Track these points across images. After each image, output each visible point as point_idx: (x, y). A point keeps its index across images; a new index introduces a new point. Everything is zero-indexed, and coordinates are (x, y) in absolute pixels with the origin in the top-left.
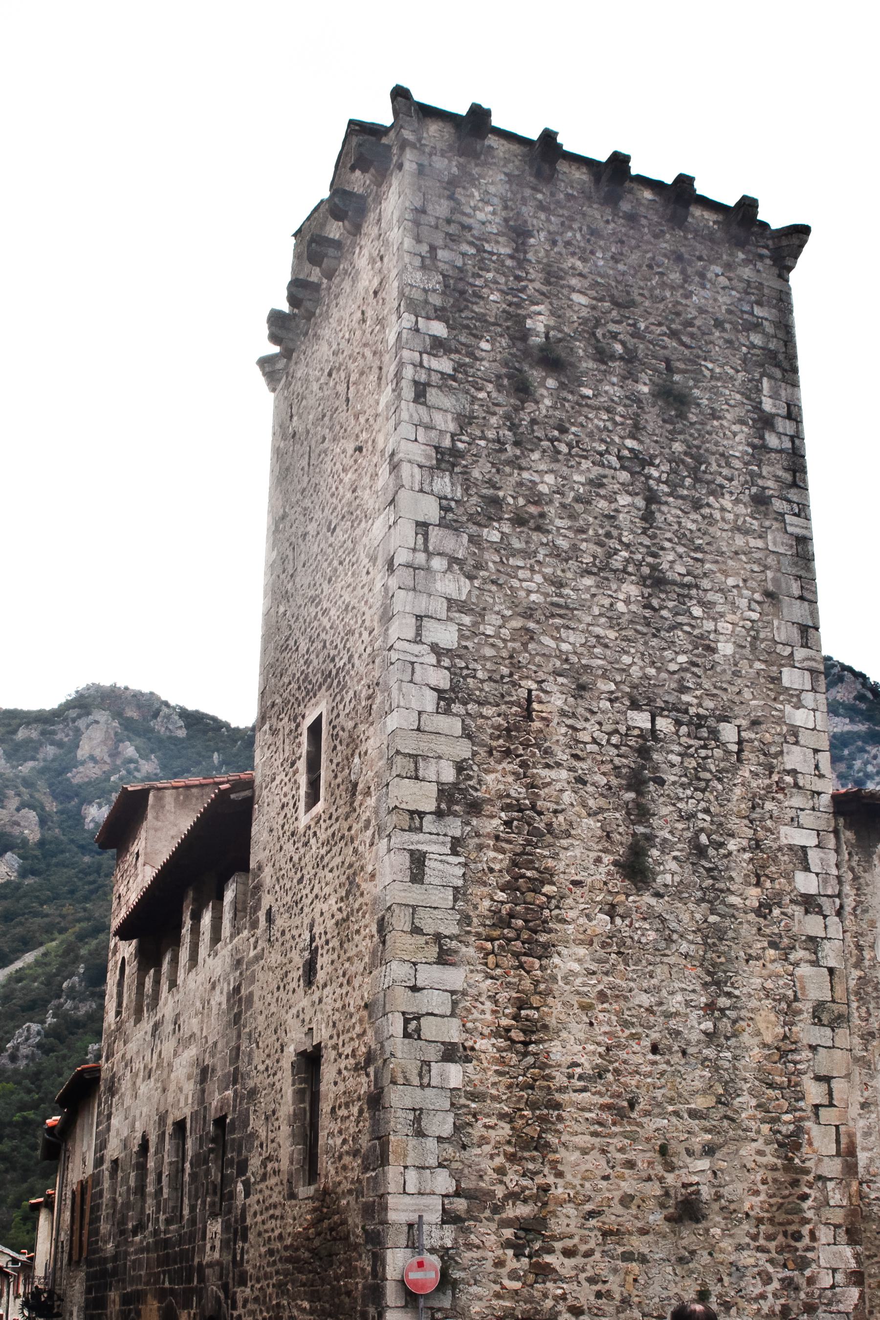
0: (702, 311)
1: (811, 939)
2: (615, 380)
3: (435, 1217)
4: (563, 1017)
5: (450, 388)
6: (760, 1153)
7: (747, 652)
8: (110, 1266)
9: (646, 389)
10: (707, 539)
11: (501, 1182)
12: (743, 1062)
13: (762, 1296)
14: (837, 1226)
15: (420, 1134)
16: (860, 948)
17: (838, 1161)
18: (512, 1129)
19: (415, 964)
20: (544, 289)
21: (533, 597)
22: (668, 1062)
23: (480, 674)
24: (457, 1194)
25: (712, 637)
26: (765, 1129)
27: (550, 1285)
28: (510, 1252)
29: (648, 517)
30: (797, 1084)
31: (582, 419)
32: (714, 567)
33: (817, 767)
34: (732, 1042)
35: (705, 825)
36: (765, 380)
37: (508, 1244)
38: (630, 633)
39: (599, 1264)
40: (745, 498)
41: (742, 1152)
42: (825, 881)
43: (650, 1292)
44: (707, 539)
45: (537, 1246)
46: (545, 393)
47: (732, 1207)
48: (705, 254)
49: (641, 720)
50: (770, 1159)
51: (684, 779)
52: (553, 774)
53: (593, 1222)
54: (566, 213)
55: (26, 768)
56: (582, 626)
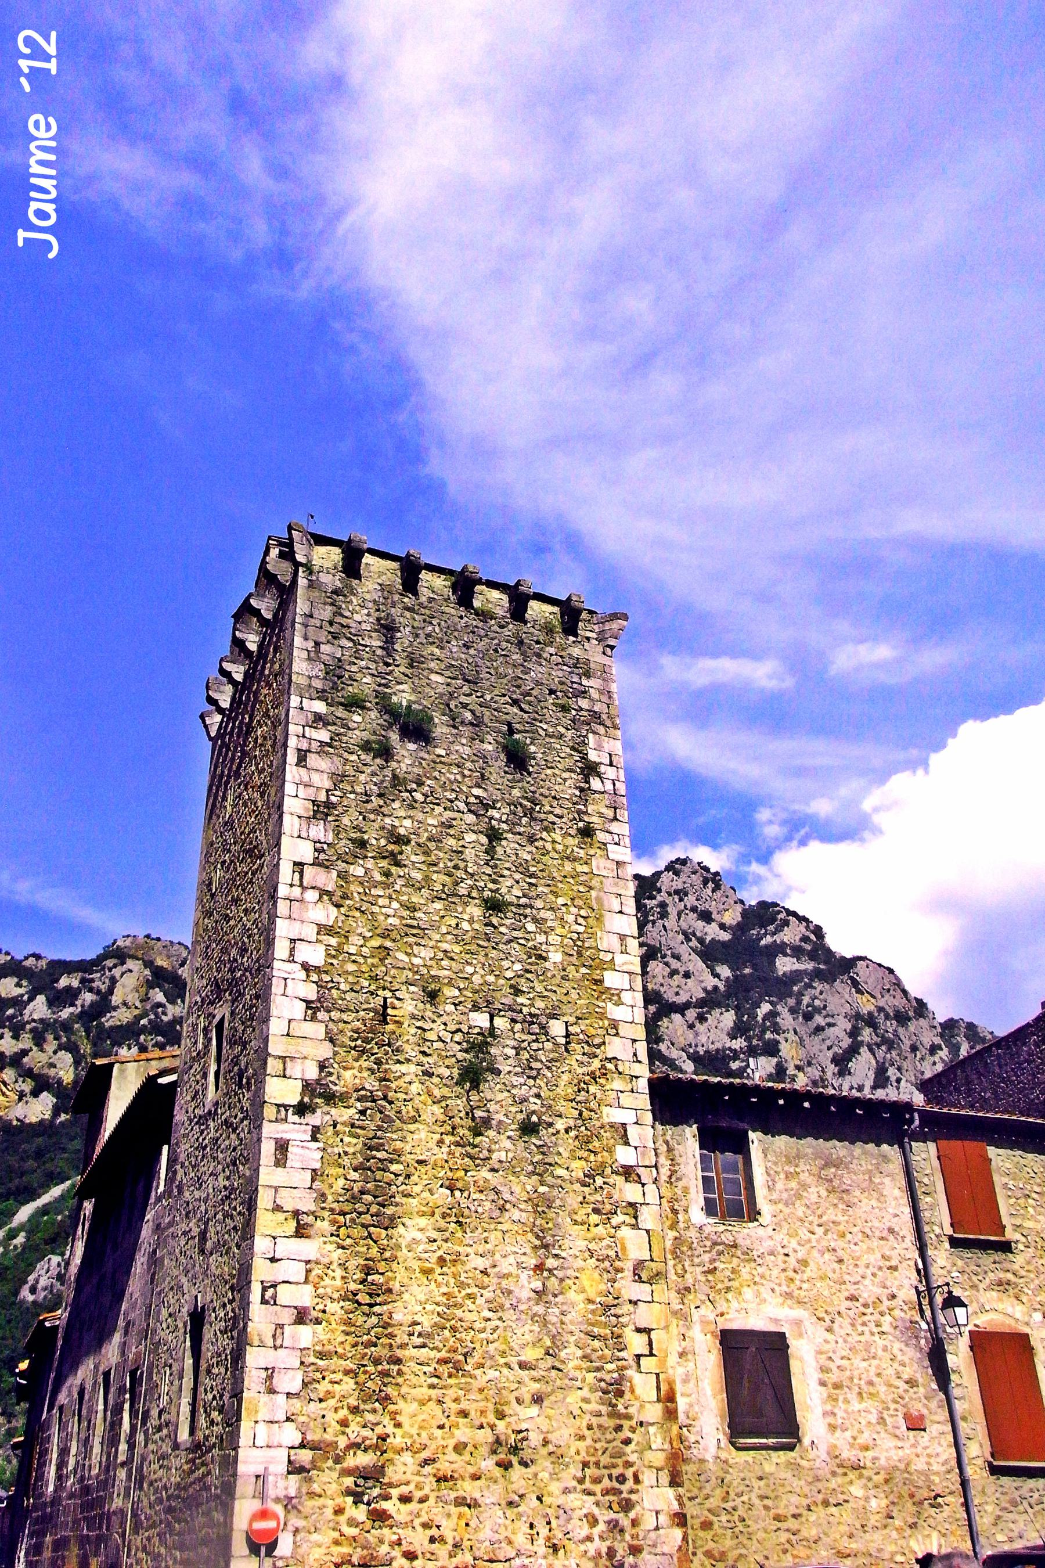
0: (538, 683)
1: (632, 1205)
2: (464, 741)
3: (283, 1467)
4: (406, 1281)
5: (327, 753)
6: (586, 1401)
7: (574, 959)
9: (490, 748)
10: (541, 866)
11: (343, 1433)
12: (569, 1317)
13: (589, 1539)
14: (658, 1470)
15: (272, 1391)
16: (675, 1212)
17: (659, 1407)
18: (357, 1383)
19: (274, 1238)
20: (408, 672)
21: (391, 920)
22: (500, 1319)
23: (342, 987)
24: (302, 1446)
25: (544, 947)
26: (590, 1377)
27: (386, 1531)
28: (350, 1500)
29: (490, 851)
30: (619, 1336)
31: (436, 774)
32: (546, 890)
33: (635, 1054)
34: (560, 1299)
35: (536, 1108)
36: (590, 735)
37: (349, 1492)
38: (473, 948)
39: (433, 1510)
40: (573, 832)
41: (568, 1400)
42: (643, 1154)
43: (481, 1536)
44: (541, 866)
45: (376, 1492)
46: (406, 753)
47: (559, 1452)
48: (541, 638)
49: (481, 1020)
50: (594, 1406)
51: (518, 1069)
52: (403, 1068)
53: (428, 1469)
54: (428, 612)
55: (65, 1013)
56: (431, 943)
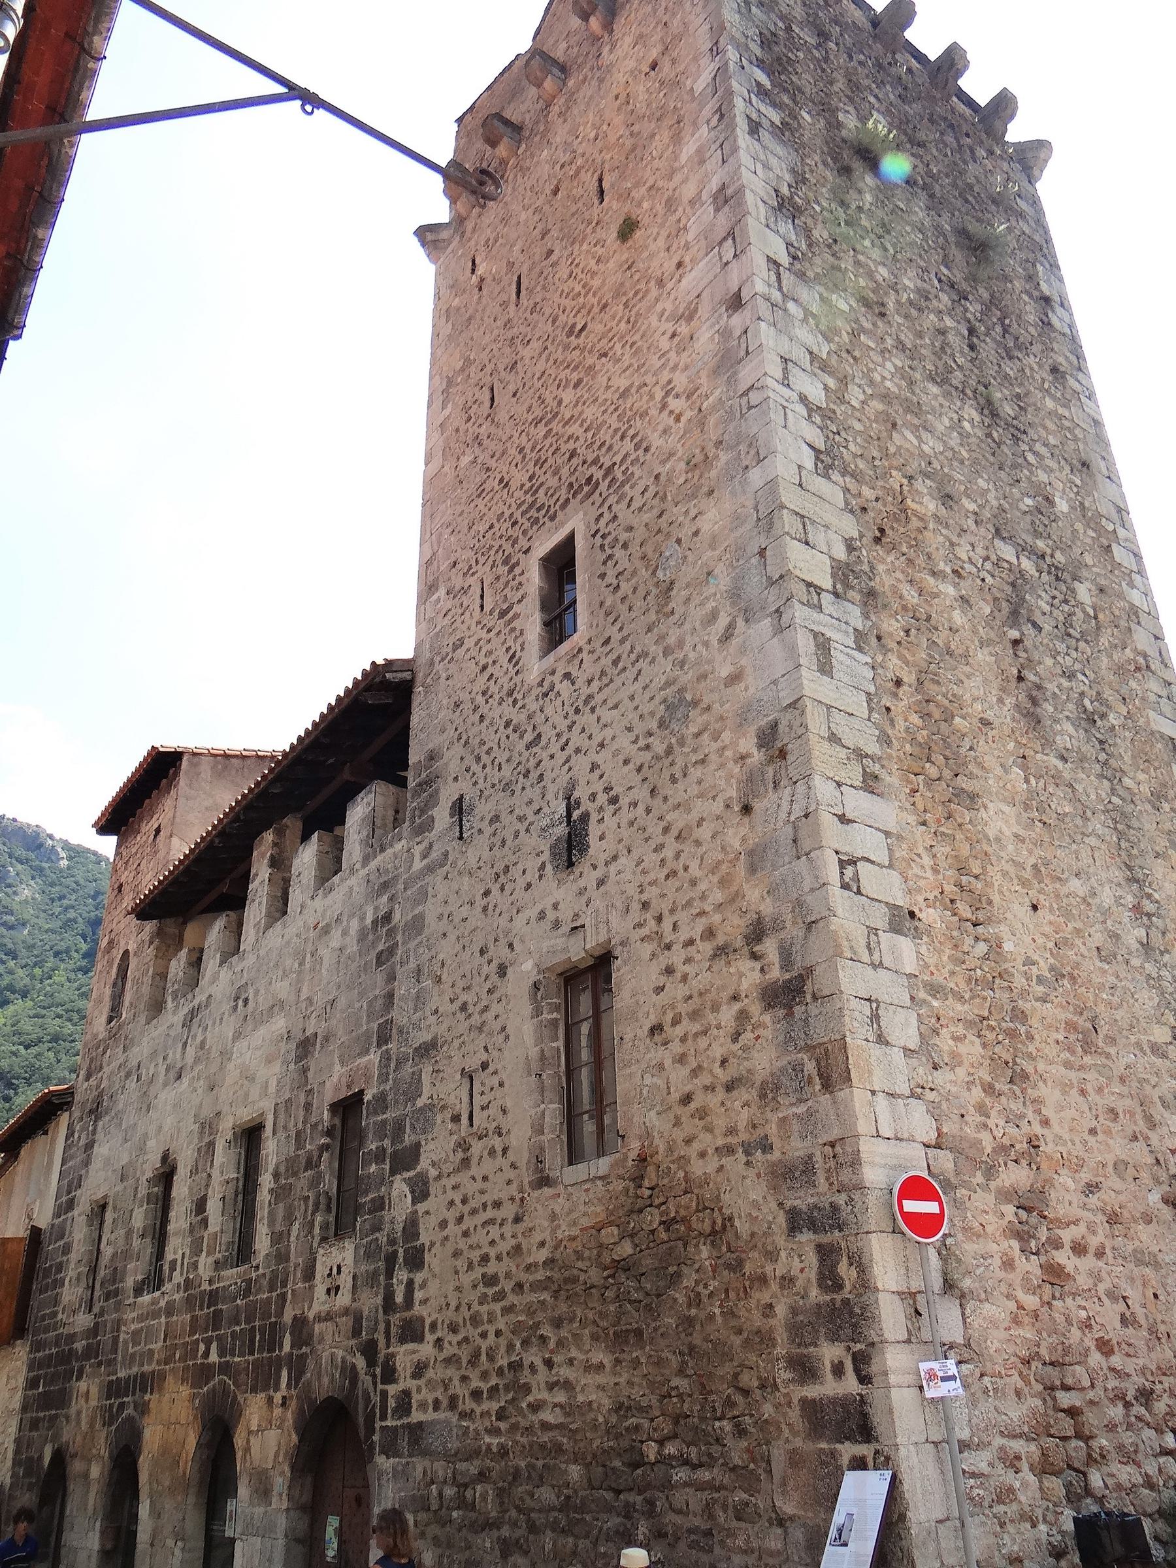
8: (79, 1345)
15: (881, 1040)
